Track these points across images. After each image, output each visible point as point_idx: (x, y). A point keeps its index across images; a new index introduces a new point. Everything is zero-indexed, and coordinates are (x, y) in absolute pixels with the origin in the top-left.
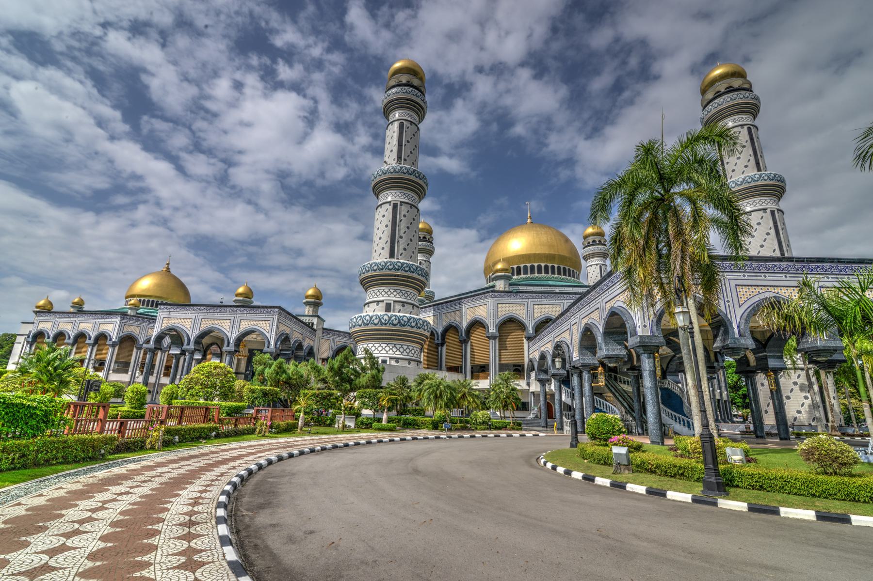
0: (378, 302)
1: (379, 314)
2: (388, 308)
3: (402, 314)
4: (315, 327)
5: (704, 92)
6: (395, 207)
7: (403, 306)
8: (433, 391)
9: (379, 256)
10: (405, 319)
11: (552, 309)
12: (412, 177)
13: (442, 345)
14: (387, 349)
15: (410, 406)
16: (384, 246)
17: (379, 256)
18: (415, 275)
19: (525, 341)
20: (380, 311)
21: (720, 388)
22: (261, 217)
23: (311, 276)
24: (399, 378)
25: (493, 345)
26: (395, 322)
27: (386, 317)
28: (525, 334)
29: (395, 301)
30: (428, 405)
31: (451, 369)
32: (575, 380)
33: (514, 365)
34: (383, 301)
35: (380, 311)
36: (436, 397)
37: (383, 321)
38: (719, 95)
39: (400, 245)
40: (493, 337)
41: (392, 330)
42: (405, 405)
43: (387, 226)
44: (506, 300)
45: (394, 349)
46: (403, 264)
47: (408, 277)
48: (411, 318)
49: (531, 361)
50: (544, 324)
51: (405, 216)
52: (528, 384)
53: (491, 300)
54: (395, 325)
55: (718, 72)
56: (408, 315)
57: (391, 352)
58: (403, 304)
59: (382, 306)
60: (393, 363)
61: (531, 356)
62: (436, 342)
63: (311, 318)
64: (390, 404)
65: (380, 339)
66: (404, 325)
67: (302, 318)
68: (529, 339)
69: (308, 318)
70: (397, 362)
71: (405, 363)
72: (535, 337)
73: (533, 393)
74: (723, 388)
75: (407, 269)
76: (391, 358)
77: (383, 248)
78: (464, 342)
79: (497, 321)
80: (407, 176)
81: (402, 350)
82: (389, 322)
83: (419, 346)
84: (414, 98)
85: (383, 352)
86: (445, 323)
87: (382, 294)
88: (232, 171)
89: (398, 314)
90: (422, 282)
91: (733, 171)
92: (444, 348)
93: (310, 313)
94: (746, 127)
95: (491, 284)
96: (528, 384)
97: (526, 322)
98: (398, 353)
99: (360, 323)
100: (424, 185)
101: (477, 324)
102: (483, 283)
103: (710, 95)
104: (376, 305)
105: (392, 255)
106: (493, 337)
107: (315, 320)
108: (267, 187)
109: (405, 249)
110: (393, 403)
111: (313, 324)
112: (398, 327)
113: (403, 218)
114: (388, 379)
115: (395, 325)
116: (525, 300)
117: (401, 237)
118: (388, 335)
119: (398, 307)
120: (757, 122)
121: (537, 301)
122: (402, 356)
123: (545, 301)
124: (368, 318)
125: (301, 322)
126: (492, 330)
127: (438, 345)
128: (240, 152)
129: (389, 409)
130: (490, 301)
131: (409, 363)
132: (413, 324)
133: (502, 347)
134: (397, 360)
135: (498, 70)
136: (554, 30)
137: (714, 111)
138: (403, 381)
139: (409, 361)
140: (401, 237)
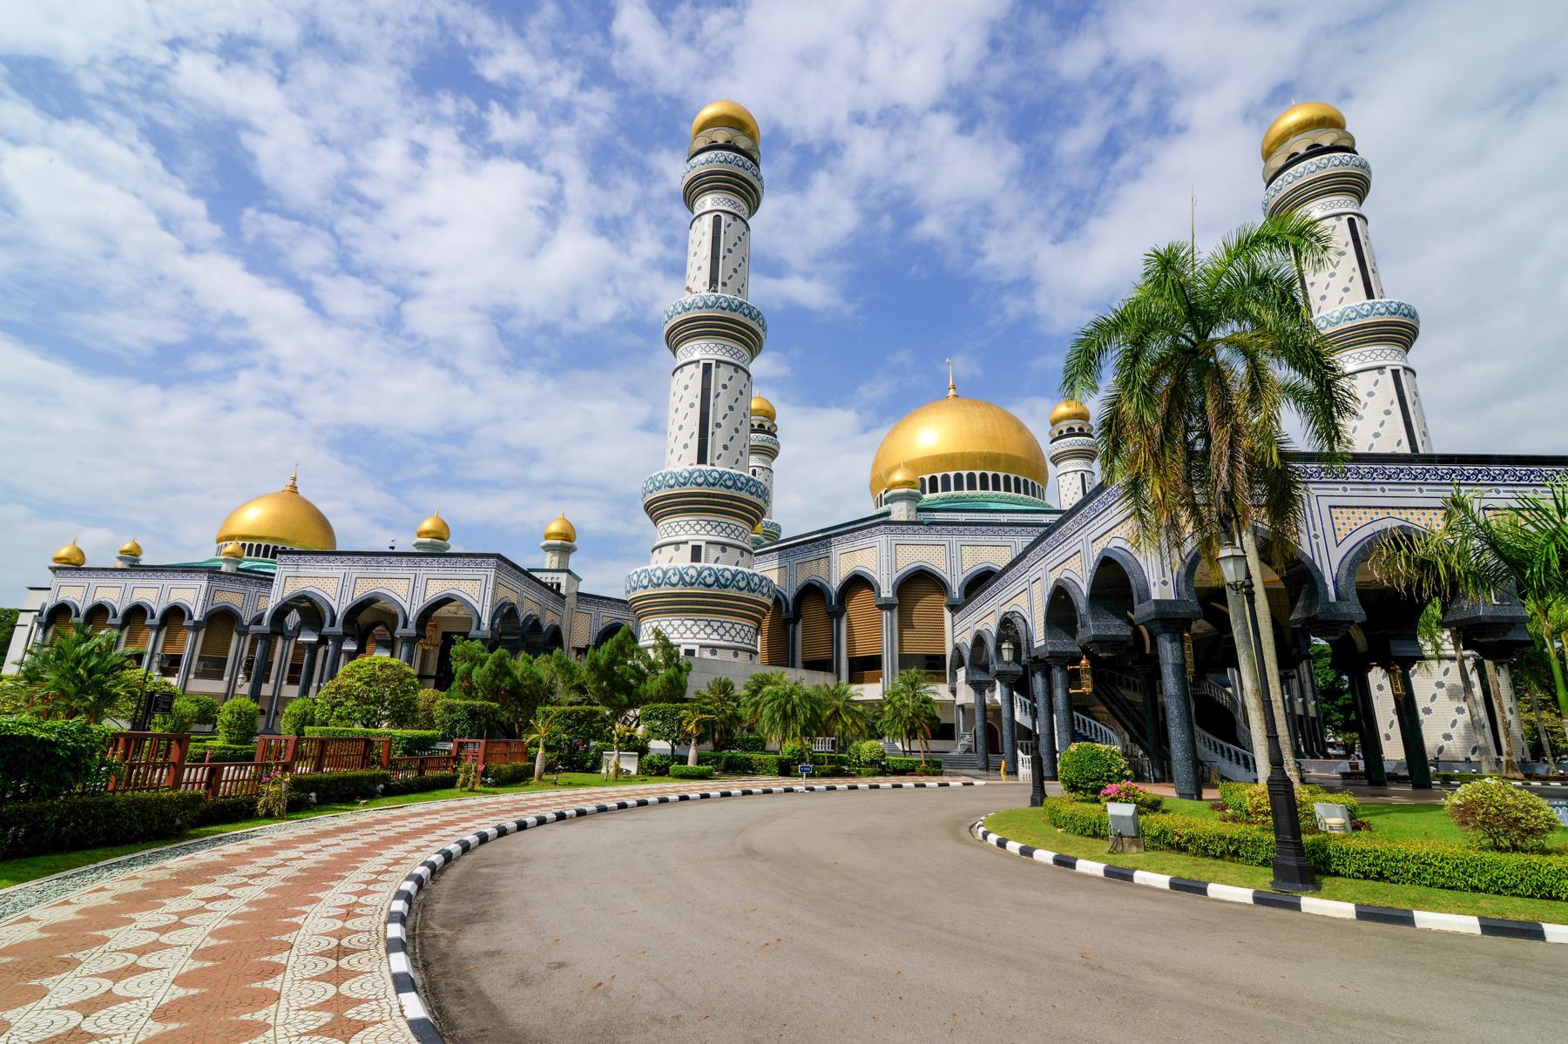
2: (696, 554)
3: (721, 566)
4: (563, 591)
6: (707, 368)
7: (724, 550)
10: (727, 574)
11: (995, 553)
12: (737, 316)
14: (695, 629)
15: (737, 733)
16: (688, 441)
17: (679, 460)
18: (744, 495)
19: (947, 614)
21: (1303, 695)
22: (463, 391)
26: (710, 580)
27: (692, 572)
28: (945, 600)
29: (708, 543)
30: (771, 731)
31: (811, 665)
32: (1038, 682)
33: (928, 657)
35: (682, 559)
36: (785, 717)
38: (1294, 160)
40: (886, 606)
42: (728, 732)
43: (692, 405)
45: (709, 630)
49: (957, 648)
50: (981, 581)
51: (725, 387)
52: (954, 692)
56: (733, 568)
57: (702, 635)
59: (686, 551)
60: (707, 654)
61: (957, 640)
62: (784, 615)
63: (556, 575)
64: (702, 730)
66: (726, 586)
67: (537, 575)
68: (954, 608)
69: (550, 575)
70: (714, 653)
71: (729, 655)
72: (966, 604)
73: (962, 707)
74: (1309, 695)
75: (730, 483)
76: (702, 646)
77: (686, 446)
79: (895, 576)
80: (727, 314)
81: (721, 631)
82: (699, 580)
83: (753, 624)
84: (741, 172)
86: (800, 582)
89: (715, 566)
91: (1323, 298)
92: (799, 627)
93: (555, 566)
94: (1345, 219)
95: (884, 509)
96: (954, 692)
98: (715, 636)
99: (645, 583)
100: (762, 334)
101: (858, 582)
102: (869, 509)
103: (1278, 161)
105: (702, 458)
106: (886, 606)
107: (563, 578)
109: (726, 447)
111: (559, 585)
112: (715, 590)
113: (721, 390)
114: (697, 684)
116: (945, 538)
117: (719, 425)
119: (715, 552)
120: (1365, 209)
121: (968, 539)
122: (722, 643)
124: (659, 573)
126: (887, 592)
127: (786, 622)
128: (423, 273)
131: (736, 655)
132: (742, 584)
133: (905, 623)
134: (714, 649)
135: (892, 118)
136: (994, 44)
139: (736, 651)
140: (719, 425)
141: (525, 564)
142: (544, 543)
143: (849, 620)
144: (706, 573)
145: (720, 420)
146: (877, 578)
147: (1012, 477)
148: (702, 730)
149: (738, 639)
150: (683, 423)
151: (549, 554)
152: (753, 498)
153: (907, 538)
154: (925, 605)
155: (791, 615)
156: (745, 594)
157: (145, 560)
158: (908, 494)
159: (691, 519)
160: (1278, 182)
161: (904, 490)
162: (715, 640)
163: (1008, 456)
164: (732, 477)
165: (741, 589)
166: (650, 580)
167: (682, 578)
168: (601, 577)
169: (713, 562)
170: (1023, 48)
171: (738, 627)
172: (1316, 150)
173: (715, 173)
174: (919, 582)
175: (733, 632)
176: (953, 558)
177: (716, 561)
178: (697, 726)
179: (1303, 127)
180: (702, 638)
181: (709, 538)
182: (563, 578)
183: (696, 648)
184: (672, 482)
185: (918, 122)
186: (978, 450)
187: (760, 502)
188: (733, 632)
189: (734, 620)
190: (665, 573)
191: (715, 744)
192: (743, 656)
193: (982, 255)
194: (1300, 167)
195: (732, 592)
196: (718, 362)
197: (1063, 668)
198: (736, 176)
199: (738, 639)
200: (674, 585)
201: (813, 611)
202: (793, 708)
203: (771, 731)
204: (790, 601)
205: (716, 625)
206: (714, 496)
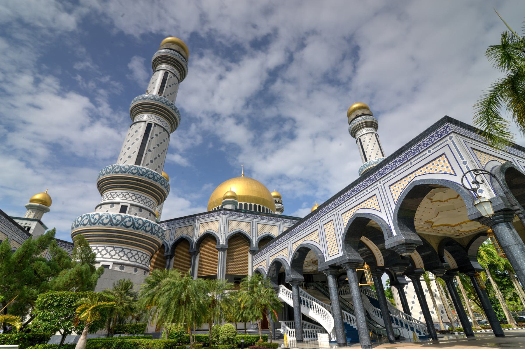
0: (112, 204)
1: (111, 214)
2: (123, 209)
3: (137, 217)
4: (31, 232)
5: (349, 115)
7: (140, 210)
8: (176, 293)
9: (127, 160)
10: (140, 222)
11: (273, 229)
12: (169, 108)
13: (171, 257)
14: (113, 253)
15: (129, 321)
17: (127, 160)
18: (157, 184)
19: (250, 256)
20: (115, 211)
22: (29, 171)
23: (61, 219)
24: (121, 282)
25: (221, 256)
26: (128, 224)
27: (119, 218)
28: (249, 249)
29: (132, 205)
30: (390, 289)
34: (119, 203)
35: (115, 211)
36: (179, 303)
37: (114, 221)
38: (358, 116)
39: (147, 157)
40: (222, 249)
41: (123, 232)
42: (121, 320)
44: (236, 217)
45: (121, 254)
46: (147, 171)
47: (151, 184)
48: (147, 222)
50: (266, 241)
51: (157, 135)
53: (223, 217)
54: (127, 227)
55: (356, 106)
56: (144, 219)
57: (117, 256)
58: (141, 208)
60: (117, 268)
62: (166, 254)
63: (29, 222)
64: (97, 317)
65: (106, 241)
66: (138, 229)
67: (17, 221)
68: (253, 253)
69: (24, 222)
70: (122, 268)
71: (131, 270)
72: (259, 251)
75: (151, 176)
76: (115, 263)
78: (194, 254)
79: (228, 235)
80: (164, 106)
81: (130, 255)
82: (122, 223)
83: (149, 254)
84: (180, 61)
85: (108, 256)
86: (177, 237)
87: (120, 197)
88: (10, 135)
89: (133, 216)
90: (163, 192)
91: (370, 156)
93: (31, 217)
94: (374, 134)
97: (251, 237)
98: (125, 258)
99: (85, 222)
100: (178, 119)
101: (209, 237)
103: (353, 116)
104: (112, 207)
105: (138, 162)
106: (222, 249)
107: (33, 225)
108: (42, 152)
109: (152, 161)
110: (101, 314)
111: (29, 228)
112: (131, 230)
113: (154, 136)
114: (103, 285)
115: (127, 227)
116: (251, 219)
117: (150, 151)
118: (122, 182)
119: (135, 210)
121: (260, 221)
122: (129, 262)
123: (266, 222)
125: (16, 224)
126: (223, 242)
127: (166, 257)
128: (24, 122)
129: (93, 329)
130: (222, 218)
131: (136, 271)
132: (148, 229)
133: (230, 258)
134: (122, 265)
135: (216, 116)
136: (247, 104)
137: (357, 123)
138: (126, 287)
139: (136, 268)
140: (150, 151)
141: (10, 214)
142: (28, 204)
143: (200, 257)
144: (127, 219)
145: (151, 149)
146: (218, 235)
147: (265, 208)
148: (97, 317)
149: (144, 263)
150: (131, 146)
151: (29, 211)
152: (162, 187)
153: (234, 218)
154: (241, 249)
155: (169, 253)
156: (148, 235)
157: (138, 208)
158: (232, 201)
159: (125, 192)
160: (352, 123)
161: (232, 199)
162: (124, 260)
163: (264, 199)
164: (152, 173)
165: (147, 231)
166: (90, 221)
167: (111, 220)
168: (61, 225)
169: (132, 214)
170: (255, 106)
171: (140, 254)
172: (363, 115)
173: (170, 57)
174: (238, 238)
175: (137, 257)
176: (255, 229)
177: (136, 215)
178: (93, 314)
179: (359, 108)
180: (116, 258)
181: (133, 203)
182: (33, 225)
183: (111, 264)
184: (117, 170)
185: (224, 119)
186: (254, 195)
187: (165, 190)
188: (137, 257)
189: (139, 249)
190: (100, 217)
191: (109, 330)
192: (140, 272)
193: (238, 160)
194: (359, 118)
195: (141, 232)
196: (156, 124)
197: (354, 271)
198: (178, 61)
199: (139, 261)
200: (104, 224)
201: (182, 252)
202: (187, 297)
203: (390, 289)
204: (170, 247)
205: (127, 251)
206: (141, 181)
